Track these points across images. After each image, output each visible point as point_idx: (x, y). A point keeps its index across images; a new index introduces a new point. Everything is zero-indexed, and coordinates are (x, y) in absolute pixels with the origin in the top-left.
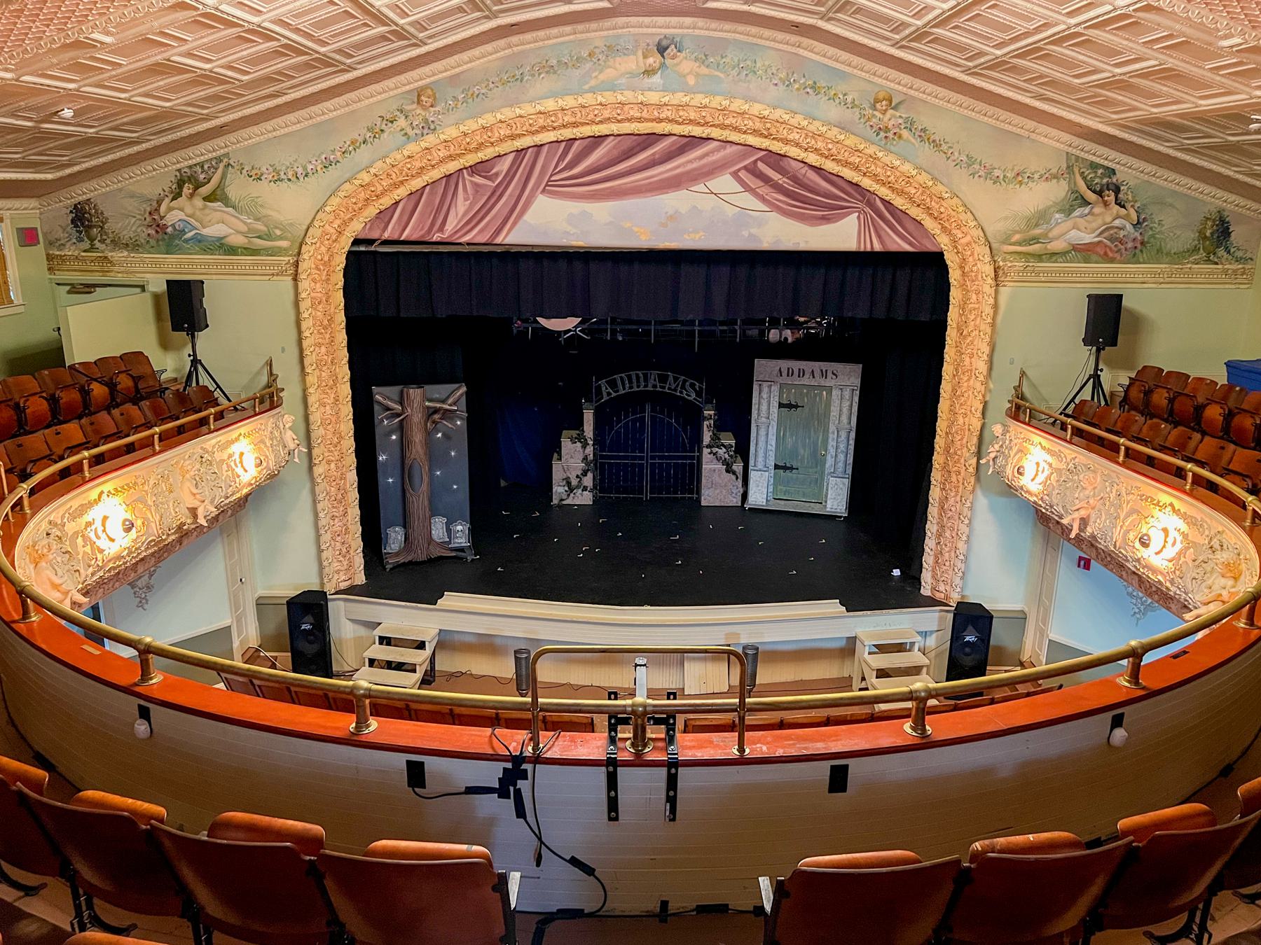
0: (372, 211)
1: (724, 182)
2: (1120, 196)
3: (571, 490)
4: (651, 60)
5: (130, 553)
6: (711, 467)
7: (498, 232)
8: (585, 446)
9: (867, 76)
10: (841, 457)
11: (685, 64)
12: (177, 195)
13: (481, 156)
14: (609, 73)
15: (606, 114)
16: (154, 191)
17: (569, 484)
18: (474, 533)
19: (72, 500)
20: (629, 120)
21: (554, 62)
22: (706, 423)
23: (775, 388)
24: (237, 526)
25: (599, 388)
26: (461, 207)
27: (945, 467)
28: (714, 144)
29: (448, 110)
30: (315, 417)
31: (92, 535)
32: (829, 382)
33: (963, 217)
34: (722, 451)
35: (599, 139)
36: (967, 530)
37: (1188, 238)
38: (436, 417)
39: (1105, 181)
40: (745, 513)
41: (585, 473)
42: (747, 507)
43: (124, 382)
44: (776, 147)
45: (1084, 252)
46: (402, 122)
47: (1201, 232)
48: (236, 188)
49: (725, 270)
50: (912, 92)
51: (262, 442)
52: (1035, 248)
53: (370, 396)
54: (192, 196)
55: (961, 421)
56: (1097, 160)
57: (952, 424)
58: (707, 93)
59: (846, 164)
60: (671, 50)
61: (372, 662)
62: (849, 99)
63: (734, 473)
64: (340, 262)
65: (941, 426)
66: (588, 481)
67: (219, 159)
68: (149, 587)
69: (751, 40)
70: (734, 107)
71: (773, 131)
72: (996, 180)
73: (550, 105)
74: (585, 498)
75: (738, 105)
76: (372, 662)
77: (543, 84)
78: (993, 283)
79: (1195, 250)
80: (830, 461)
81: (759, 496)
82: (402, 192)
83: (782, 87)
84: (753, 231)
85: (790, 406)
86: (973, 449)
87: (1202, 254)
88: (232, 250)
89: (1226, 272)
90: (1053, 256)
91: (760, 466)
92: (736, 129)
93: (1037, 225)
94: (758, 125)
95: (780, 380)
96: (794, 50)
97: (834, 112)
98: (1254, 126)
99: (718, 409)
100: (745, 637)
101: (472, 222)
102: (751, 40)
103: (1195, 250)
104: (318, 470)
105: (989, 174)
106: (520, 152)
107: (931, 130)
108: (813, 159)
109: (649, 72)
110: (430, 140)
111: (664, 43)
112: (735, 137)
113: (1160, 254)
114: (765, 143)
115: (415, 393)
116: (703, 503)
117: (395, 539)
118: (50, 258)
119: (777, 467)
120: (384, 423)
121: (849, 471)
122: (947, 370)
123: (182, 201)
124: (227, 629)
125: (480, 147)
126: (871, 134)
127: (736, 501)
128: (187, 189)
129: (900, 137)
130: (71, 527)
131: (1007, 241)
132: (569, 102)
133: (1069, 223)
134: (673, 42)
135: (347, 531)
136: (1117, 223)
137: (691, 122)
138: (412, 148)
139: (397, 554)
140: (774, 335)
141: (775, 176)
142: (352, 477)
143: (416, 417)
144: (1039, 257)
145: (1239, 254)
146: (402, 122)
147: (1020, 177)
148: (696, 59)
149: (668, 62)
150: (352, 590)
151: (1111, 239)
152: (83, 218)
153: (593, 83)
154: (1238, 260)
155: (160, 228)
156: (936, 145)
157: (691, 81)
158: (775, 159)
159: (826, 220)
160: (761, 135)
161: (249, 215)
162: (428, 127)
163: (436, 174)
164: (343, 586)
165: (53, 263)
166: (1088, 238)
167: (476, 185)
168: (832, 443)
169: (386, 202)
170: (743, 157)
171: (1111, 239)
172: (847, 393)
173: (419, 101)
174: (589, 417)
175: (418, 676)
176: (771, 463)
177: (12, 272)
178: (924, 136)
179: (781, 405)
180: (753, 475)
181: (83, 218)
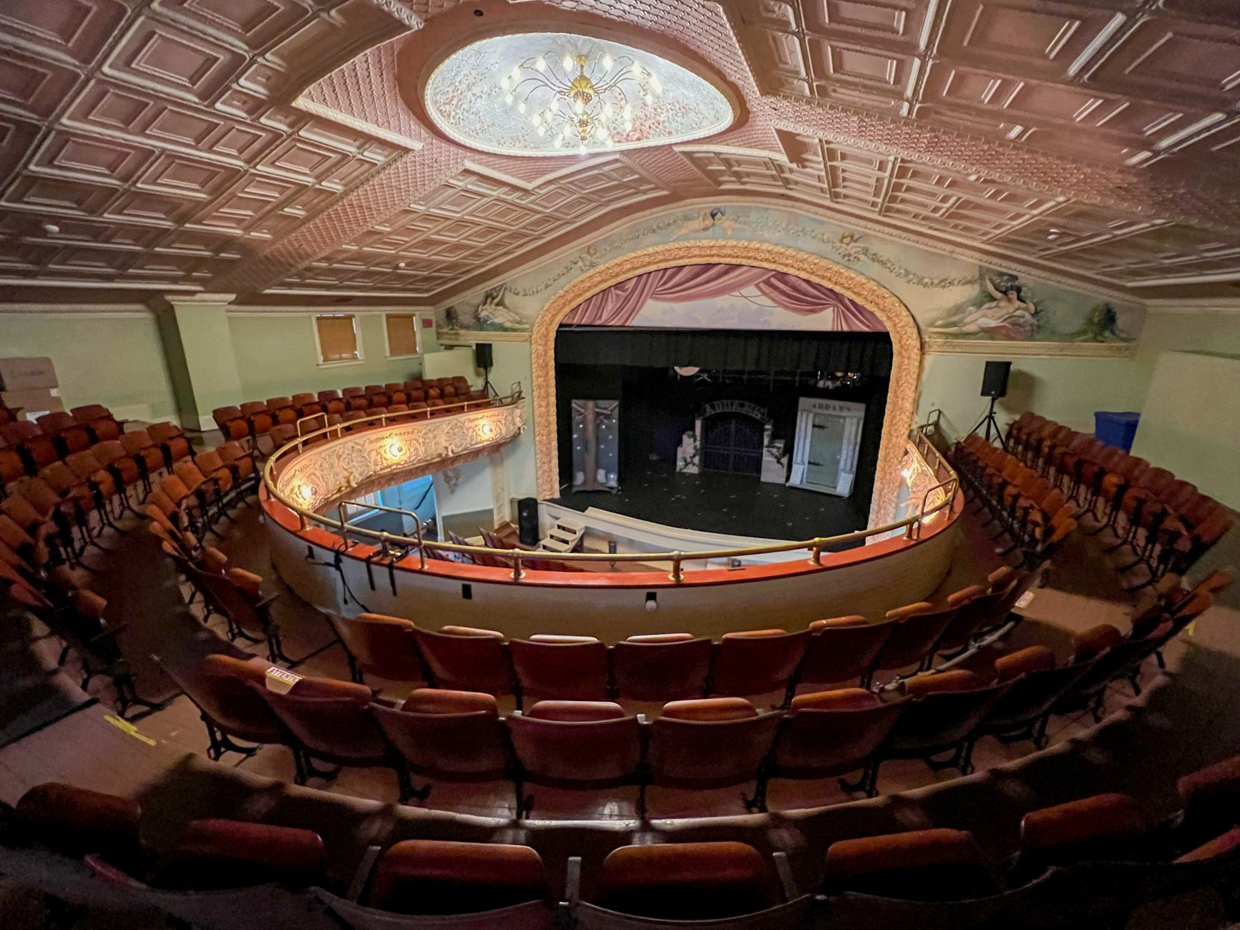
0: (567, 309)
1: (751, 290)
2: (1022, 294)
3: (687, 464)
4: (707, 222)
5: (406, 462)
6: (768, 459)
7: (627, 320)
8: (695, 441)
9: (837, 222)
10: (849, 461)
11: (725, 222)
12: (485, 303)
13: (619, 279)
14: (684, 231)
15: (681, 253)
16: (476, 301)
17: (685, 461)
18: (620, 480)
19: (372, 434)
20: (695, 256)
21: (655, 227)
22: (766, 433)
23: (811, 416)
24: (502, 461)
25: (705, 409)
26: (610, 307)
28: (745, 268)
30: (537, 413)
31: (383, 453)
32: (844, 414)
33: (898, 309)
34: (774, 450)
35: (682, 267)
36: (894, 511)
37: (1078, 323)
38: (602, 417)
39: (1009, 284)
40: (787, 491)
41: (694, 456)
42: (787, 485)
43: (450, 389)
44: (781, 269)
45: (990, 333)
46: (580, 264)
48: (509, 299)
49: (815, 344)
50: (867, 231)
51: (500, 421)
52: (954, 330)
53: (570, 409)
56: (1003, 270)
57: (889, 441)
58: (736, 239)
59: (823, 277)
60: (719, 215)
61: (552, 537)
62: (825, 237)
63: (781, 464)
64: (553, 335)
66: (696, 460)
67: (502, 285)
68: (455, 485)
69: (764, 206)
70: (752, 246)
71: (777, 259)
72: (925, 285)
73: (651, 250)
74: (694, 470)
75: (756, 245)
76: (552, 537)
77: (652, 238)
78: (919, 352)
79: (1083, 332)
80: (842, 463)
81: (795, 480)
82: (581, 300)
83: (783, 233)
84: (767, 318)
85: (820, 427)
88: (506, 330)
89: (1110, 348)
90: (967, 335)
93: (955, 314)
94: (768, 256)
95: (814, 410)
96: (791, 210)
97: (814, 246)
98: (1051, 237)
99: (774, 426)
100: (617, 532)
101: (616, 313)
102: (764, 206)
103: (1083, 332)
105: (920, 282)
106: (640, 276)
107: (880, 254)
108: (803, 275)
109: (705, 229)
110: (592, 272)
111: (715, 212)
112: (755, 263)
113: (1053, 335)
114: (773, 266)
115: (591, 404)
116: (763, 479)
117: (579, 478)
118: (438, 333)
119: (809, 463)
121: (854, 469)
122: (888, 407)
124: (491, 511)
125: (617, 275)
126: (839, 259)
127: (781, 480)
129: (859, 260)
130: (368, 447)
131: (932, 325)
132: (660, 248)
133: (980, 313)
134: (719, 210)
135: (551, 471)
137: (729, 256)
138: (583, 276)
139: (579, 486)
140: (821, 384)
141: (781, 286)
143: (590, 416)
144: (956, 336)
145: (1124, 335)
147: (944, 283)
148: (733, 220)
149: (716, 222)
150: (552, 501)
152: (450, 315)
153: (675, 237)
154: (1124, 340)
155: (477, 318)
156: (883, 263)
157: (729, 232)
158: (782, 276)
159: (812, 311)
160: (770, 262)
162: (592, 265)
163: (597, 290)
164: (548, 498)
165: (439, 335)
166: (993, 323)
167: (617, 295)
168: (844, 452)
169: (574, 305)
170: (763, 274)
171: (1014, 324)
172: (855, 421)
173: (588, 252)
174: (698, 424)
175: (571, 546)
176: (806, 461)
177: (418, 338)
178: (875, 258)
179: (814, 426)
180: (795, 467)
181: (450, 315)
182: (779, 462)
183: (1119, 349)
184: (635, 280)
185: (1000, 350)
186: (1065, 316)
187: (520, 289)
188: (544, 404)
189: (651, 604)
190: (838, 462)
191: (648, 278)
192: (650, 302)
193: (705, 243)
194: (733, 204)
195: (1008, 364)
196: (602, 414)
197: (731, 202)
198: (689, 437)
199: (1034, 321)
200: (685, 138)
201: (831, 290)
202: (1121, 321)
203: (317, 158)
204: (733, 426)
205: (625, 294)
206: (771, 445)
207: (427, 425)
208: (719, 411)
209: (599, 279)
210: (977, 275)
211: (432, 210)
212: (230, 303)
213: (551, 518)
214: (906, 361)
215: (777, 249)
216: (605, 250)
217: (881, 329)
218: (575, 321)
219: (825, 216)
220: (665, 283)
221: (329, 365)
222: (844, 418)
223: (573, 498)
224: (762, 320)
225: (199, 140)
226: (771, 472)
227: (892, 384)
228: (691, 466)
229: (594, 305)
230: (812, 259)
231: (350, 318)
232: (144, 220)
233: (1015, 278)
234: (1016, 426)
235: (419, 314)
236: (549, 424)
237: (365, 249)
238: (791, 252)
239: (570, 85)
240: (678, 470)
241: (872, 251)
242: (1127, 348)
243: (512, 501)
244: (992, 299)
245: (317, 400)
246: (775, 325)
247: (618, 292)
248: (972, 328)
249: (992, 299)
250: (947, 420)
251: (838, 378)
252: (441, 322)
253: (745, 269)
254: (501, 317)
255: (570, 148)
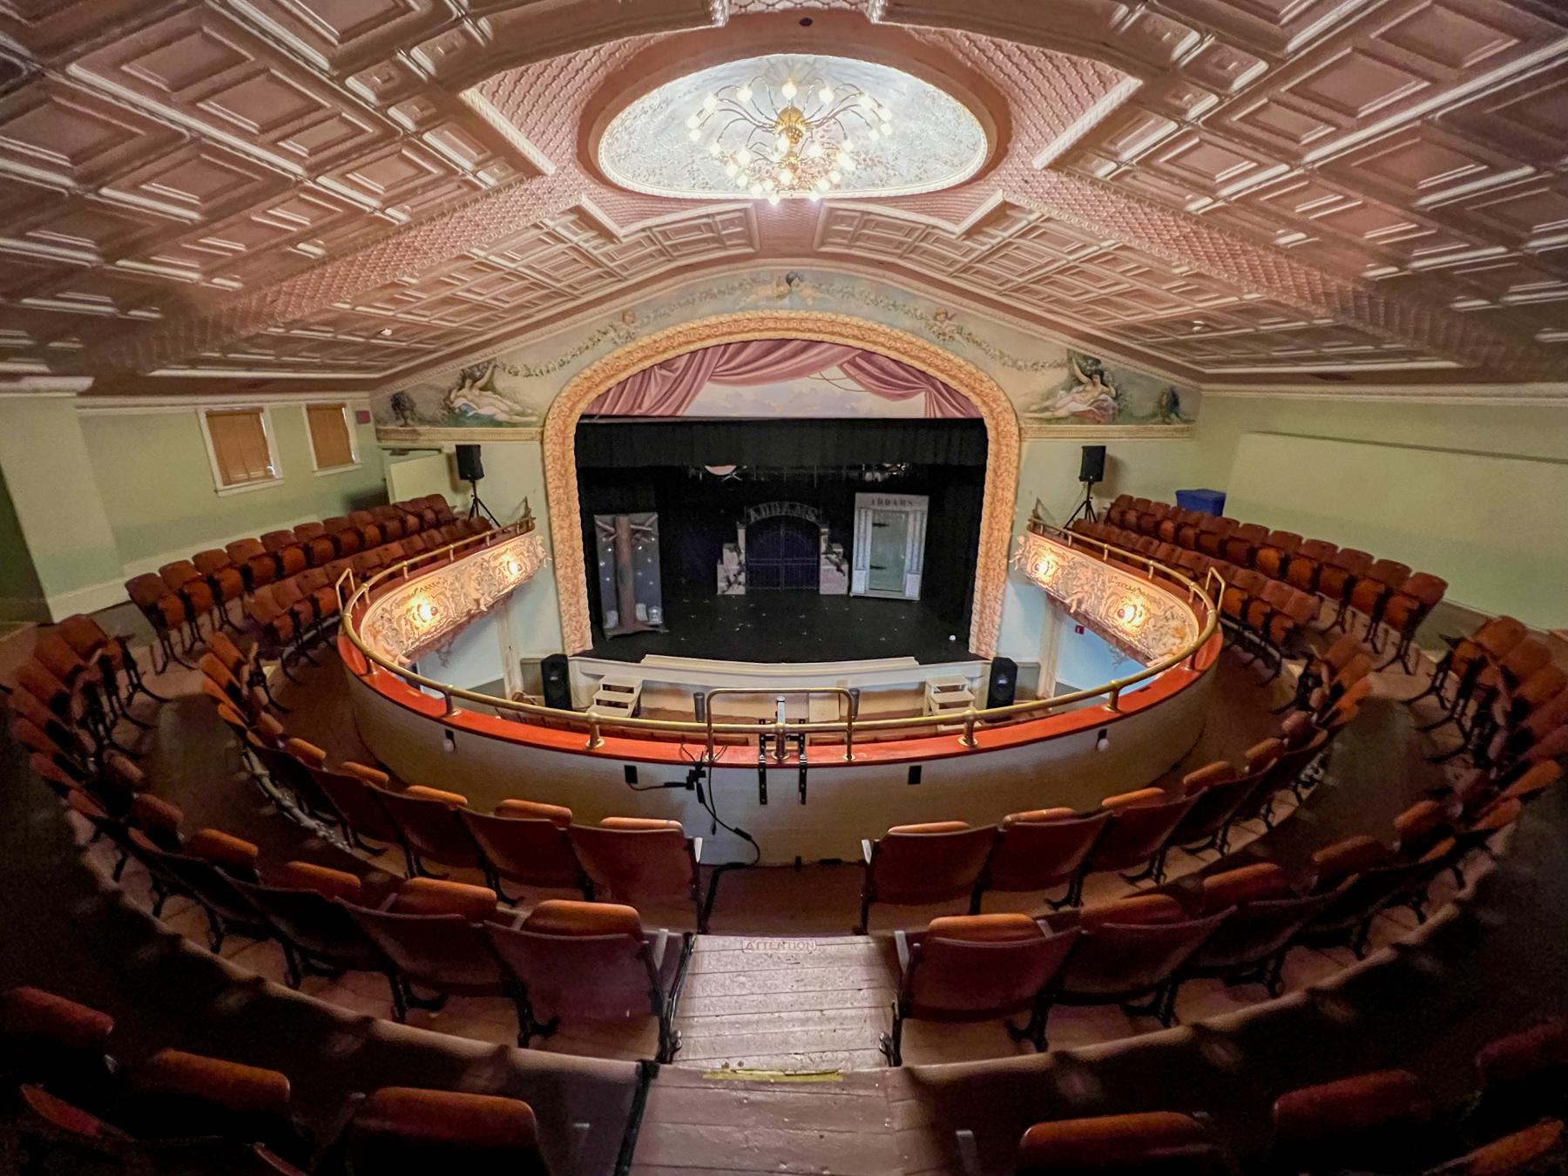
0: (593, 395)
1: (834, 372)
3: (730, 584)
4: (782, 288)
6: (826, 567)
10: (915, 560)
11: (805, 290)
12: (461, 387)
13: (667, 356)
14: (753, 297)
16: (445, 384)
17: (729, 581)
18: (665, 615)
21: (715, 290)
22: (822, 538)
23: (870, 514)
26: (653, 391)
27: (986, 566)
28: (825, 346)
29: (643, 325)
30: (557, 537)
31: (411, 618)
32: (907, 508)
34: (833, 557)
35: (746, 343)
37: (1150, 406)
38: (638, 535)
40: (848, 599)
41: (739, 573)
44: (869, 347)
45: (1079, 417)
46: (612, 334)
47: (1160, 402)
48: (501, 382)
53: (593, 525)
54: (472, 387)
55: (996, 533)
58: (820, 310)
60: (796, 281)
61: (598, 702)
62: (918, 313)
64: (572, 431)
65: (983, 537)
66: (742, 578)
67: (489, 362)
68: (449, 653)
72: (1019, 368)
73: (713, 320)
74: (739, 590)
76: (598, 702)
79: (1154, 415)
80: (907, 563)
81: (859, 587)
85: (880, 525)
86: (1005, 553)
87: (1160, 418)
88: (499, 424)
89: (1176, 430)
90: (1058, 420)
91: (860, 565)
92: (842, 335)
93: (1048, 399)
94: (856, 332)
97: (908, 322)
98: (1196, 328)
103: (1154, 415)
104: (560, 573)
105: (1015, 363)
106: (693, 353)
107: (974, 333)
108: (894, 355)
109: (780, 297)
110: (631, 346)
113: (1132, 418)
116: (822, 592)
117: (611, 619)
118: (378, 431)
119: (872, 567)
120: (602, 539)
123: (465, 391)
124: (501, 681)
126: (934, 337)
127: (844, 591)
128: (468, 383)
130: (397, 613)
132: (725, 318)
136: (1102, 397)
138: (619, 352)
140: (868, 476)
142: (583, 577)
143: (624, 536)
144: (1049, 421)
146: (612, 334)
149: (794, 289)
150: (583, 654)
151: (1098, 408)
154: (1186, 422)
155: (451, 409)
156: (979, 344)
157: (810, 302)
158: (868, 355)
159: (903, 396)
161: (509, 399)
162: (630, 337)
166: (1083, 408)
167: (664, 377)
168: (909, 551)
169: (602, 389)
172: (919, 515)
173: (624, 319)
174: (741, 533)
176: (868, 565)
177: (353, 442)
179: (874, 525)
180: (855, 573)
181: (399, 404)
182: (839, 570)
183: (1182, 430)
184: (687, 357)
185: (1095, 434)
186: (1141, 400)
187: (519, 367)
188: (566, 525)
189: (1104, 743)
190: (903, 562)
191: (705, 355)
192: (708, 386)
193: (784, 314)
194: (814, 268)
195: (1103, 448)
196: (638, 531)
197: (812, 265)
198: (731, 550)
199: (1115, 404)
200: (858, 195)
201: (923, 373)
202: (1184, 405)
203: (411, 172)
204: (782, 532)
205: (674, 376)
206: (829, 551)
207: (453, 570)
208: (764, 515)
209: (640, 355)
210: (1065, 358)
211: (491, 258)
212: (82, 394)
213: (580, 676)
214: (1004, 449)
215: (869, 324)
216: (648, 317)
217: (975, 415)
218: (603, 412)
219: (918, 289)
220: (727, 362)
221: (235, 489)
222: (907, 513)
223: (609, 645)
224: (848, 406)
225: (265, 129)
226: (830, 582)
227: (989, 475)
228: (735, 586)
229: (632, 389)
230: (909, 337)
231: (256, 412)
232: (40, 247)
233: (1098, 362)
234: (1141, 508)
235: (353, 402)
236: (574, 550)
237: (358, 308)
238: (884, 328)
239: (775, 118)
240: (719, 593)
241: (965, 331)
242: (1188, 430)
243: (524, 664)
244: (1080, 383)
245: (263, 550)
246: (862, 413)
247: (664, 372)
248: (1062, 413)
249: (1080, 383)
250: (1045, 509)
251: (887, 469)
252: (383, 414)
253: (825, 346)
254: (489, 406)
255: (707, 190)
